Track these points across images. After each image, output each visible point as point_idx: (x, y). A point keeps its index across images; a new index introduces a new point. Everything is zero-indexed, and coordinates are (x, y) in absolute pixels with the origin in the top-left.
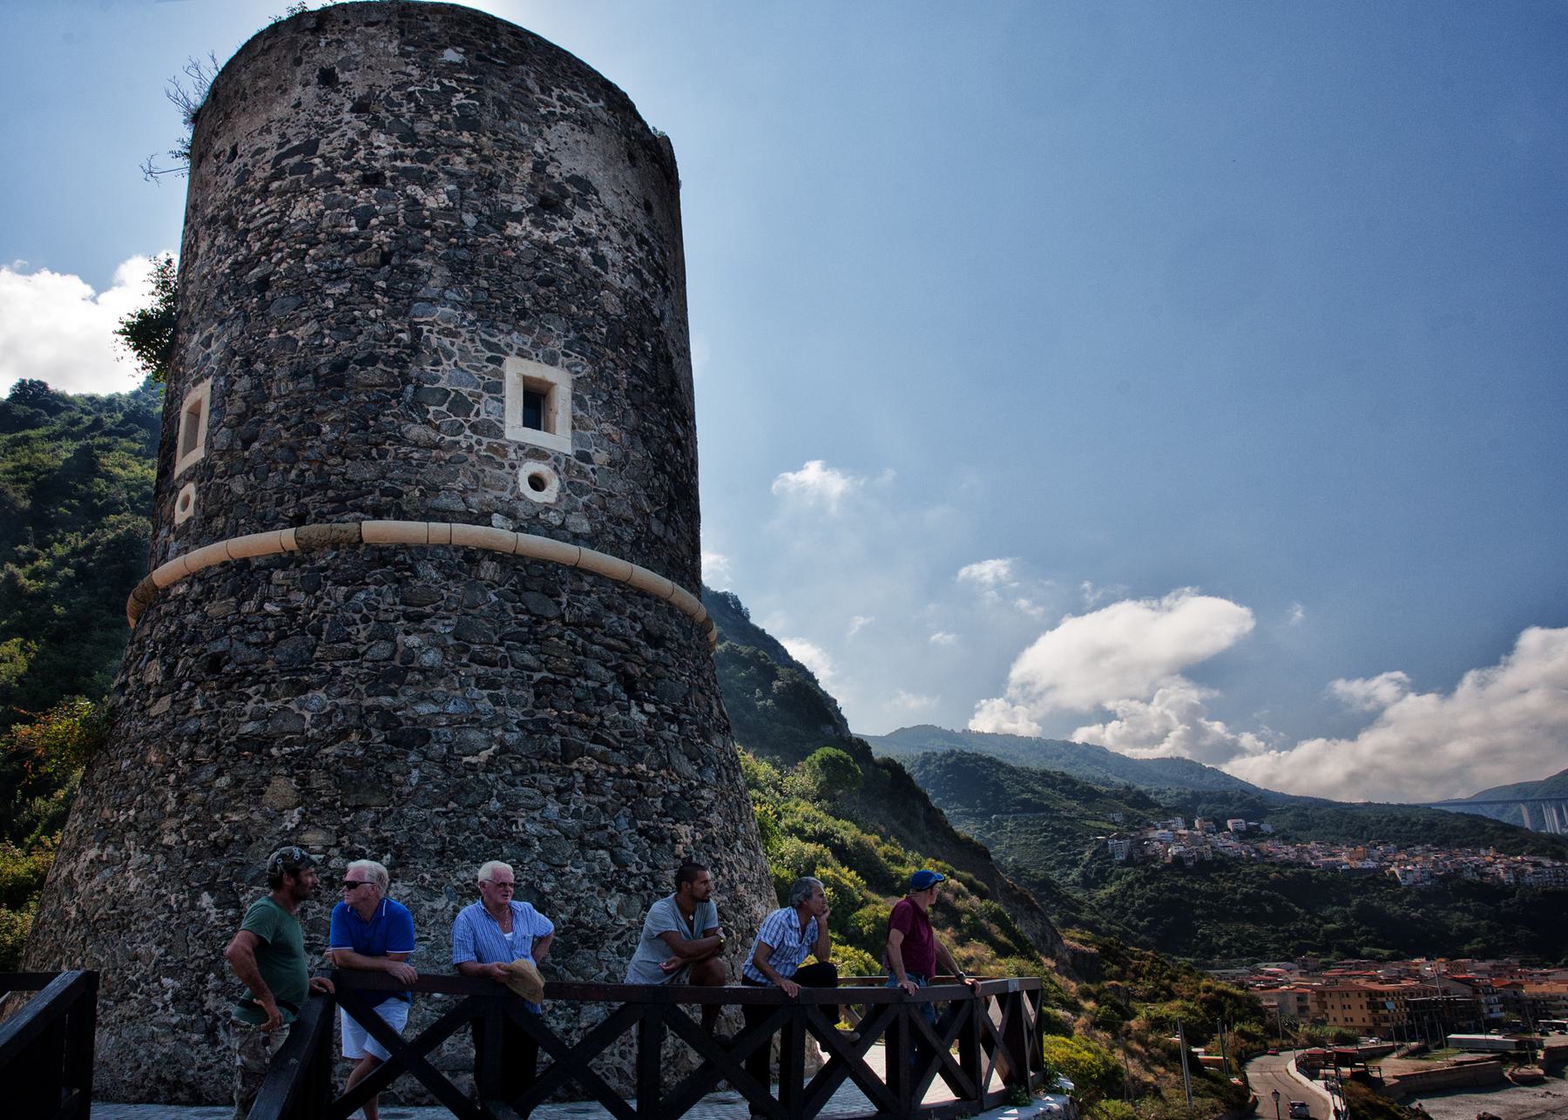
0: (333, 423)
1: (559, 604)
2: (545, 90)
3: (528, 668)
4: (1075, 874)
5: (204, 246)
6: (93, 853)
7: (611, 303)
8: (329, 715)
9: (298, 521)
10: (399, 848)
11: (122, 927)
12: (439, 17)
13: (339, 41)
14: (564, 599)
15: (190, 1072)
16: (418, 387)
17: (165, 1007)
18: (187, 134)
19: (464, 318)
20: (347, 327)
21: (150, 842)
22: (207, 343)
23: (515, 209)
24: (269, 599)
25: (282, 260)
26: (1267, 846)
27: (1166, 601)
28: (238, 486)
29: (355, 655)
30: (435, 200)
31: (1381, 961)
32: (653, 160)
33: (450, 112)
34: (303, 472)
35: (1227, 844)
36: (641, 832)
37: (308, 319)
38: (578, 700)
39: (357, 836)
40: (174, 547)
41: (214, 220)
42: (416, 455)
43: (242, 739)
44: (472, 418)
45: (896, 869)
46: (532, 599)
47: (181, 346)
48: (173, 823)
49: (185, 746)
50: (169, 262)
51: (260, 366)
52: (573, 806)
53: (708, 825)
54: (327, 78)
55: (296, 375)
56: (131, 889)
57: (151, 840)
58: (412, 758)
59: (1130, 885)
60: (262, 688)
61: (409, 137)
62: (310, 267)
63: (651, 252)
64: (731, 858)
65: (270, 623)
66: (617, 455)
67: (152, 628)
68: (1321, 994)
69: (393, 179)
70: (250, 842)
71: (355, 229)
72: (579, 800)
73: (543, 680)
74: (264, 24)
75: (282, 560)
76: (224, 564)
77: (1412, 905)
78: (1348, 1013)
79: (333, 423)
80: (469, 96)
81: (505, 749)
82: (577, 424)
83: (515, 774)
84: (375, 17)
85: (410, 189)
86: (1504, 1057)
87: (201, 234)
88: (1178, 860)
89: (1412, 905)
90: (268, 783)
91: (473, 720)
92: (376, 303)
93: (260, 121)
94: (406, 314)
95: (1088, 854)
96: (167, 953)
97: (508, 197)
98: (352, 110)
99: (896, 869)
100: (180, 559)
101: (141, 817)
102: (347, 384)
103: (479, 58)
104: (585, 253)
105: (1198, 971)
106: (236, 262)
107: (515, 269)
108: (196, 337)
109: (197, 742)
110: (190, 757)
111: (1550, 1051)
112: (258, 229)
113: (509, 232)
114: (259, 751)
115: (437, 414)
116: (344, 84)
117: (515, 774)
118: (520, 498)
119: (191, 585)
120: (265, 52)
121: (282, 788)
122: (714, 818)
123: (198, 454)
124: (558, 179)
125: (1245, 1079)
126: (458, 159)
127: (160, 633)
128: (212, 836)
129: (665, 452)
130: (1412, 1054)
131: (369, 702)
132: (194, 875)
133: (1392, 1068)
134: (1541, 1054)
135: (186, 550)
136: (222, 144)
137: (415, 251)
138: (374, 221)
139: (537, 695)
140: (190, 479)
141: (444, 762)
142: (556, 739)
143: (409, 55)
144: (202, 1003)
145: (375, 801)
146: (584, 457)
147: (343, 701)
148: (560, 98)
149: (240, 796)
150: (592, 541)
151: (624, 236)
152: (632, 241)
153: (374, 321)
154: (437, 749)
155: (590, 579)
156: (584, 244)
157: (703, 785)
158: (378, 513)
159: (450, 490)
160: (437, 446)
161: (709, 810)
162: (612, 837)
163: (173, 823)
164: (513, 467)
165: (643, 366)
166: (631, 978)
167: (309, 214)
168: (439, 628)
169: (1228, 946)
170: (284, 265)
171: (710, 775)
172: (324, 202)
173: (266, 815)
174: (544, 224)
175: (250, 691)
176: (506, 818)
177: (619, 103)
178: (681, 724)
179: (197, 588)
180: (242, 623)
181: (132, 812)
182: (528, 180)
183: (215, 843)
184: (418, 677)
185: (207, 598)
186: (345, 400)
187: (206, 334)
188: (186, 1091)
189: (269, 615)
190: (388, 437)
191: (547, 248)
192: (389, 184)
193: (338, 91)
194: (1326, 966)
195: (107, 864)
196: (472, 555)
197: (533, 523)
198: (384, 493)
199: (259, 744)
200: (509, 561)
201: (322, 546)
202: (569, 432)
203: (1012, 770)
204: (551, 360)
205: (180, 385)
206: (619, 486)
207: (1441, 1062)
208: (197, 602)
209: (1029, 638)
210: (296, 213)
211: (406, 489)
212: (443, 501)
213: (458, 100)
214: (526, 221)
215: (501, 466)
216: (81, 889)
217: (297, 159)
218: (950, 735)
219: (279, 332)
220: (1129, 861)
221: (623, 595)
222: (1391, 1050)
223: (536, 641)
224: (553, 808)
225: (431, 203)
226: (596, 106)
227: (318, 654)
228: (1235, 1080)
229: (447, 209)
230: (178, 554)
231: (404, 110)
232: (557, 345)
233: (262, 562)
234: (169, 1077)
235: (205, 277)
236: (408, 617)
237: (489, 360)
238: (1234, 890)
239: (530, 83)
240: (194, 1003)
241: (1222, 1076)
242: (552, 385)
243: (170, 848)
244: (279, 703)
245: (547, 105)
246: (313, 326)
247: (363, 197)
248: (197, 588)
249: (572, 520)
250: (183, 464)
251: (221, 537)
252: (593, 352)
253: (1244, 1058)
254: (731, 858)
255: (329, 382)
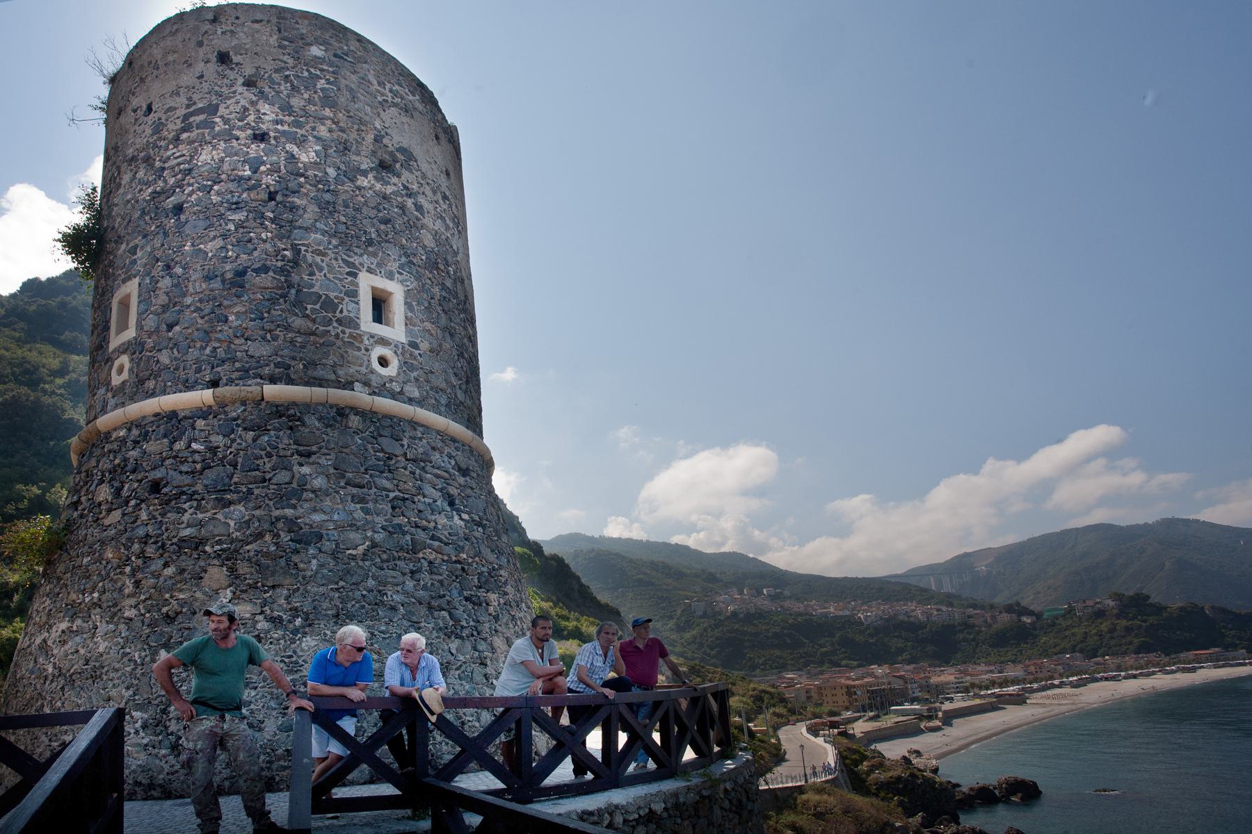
0: (237, 314)
1: (402, 446)
2: (381, 84)
3: (385, 489)
4: (671, 624)
5: (126, 178)
6: (64, 625)
7: (429, 241)
8: (248, 523)
9: (214, 384)
10: (307, 614)
11: (95, 677)
12: (306, 22)
13: (232, 32)
14: (405, 442)
15: (161, 777)
16: (298, 291)
17: (137, 732)
18: (105, 92)
19: (330, 243)
20: (245, 243)
21: (114, 614)
22: (133, 251)
23: (363, 167)
24: (195, 440)
25: (193, 192)
26: (787, 604)
27: (731, 451)
28: (164, 358)
29: (264, 480)
30: (307, 156)
31: (852, 668)
32: (450, 141)
33: (315, 92)
34: (215, 348)
35: (764, 603)
36: (467, 599)
37: (215, 238)
38: (420, 511)
39: (275, 606)
40: (112, 402)
41: (134, 159)
42: (299, 340)
43: (182, 540)
44: (338, 314)
45: (564, 623)
46: (386, 442)
47: (109, 253)
48: (132, 601)
49: (136, 546)
50: (94, 189)
51: (178, 270)
52: (422, 583)
53: (506, 594)
54: (223, 58)
55: (208, 278)
56: (101, 649)
57: (115, 614)
58: (312, 551)
59: (705, 630)
60: (195, 504)
61: (287, 108)
62: (215, 199)
63: (450, 205)
64: (521, 615)
65: (197, 457)
66: (435, 345)
67: (98, 461)
68: (819, 688)
69: (275, 138)
70: (195, 613)
71: (248, 173)
72: (426, 578)
73: (396, 498)
74: (172, 13)
75: (204, 412)
76: (156, 415)
77: (871, 636)
78: (835, 699)
79: (237, 314)
80: (328, 82)
81: (374, 545)
82: (408, 322)
83: (382, 561)
84: (259, 16)
85: (288, 147)
86: (921, 717)
87: (123, 169)
88: (734, 614)
89: (871, 636)
90: (206, 571)
91: (352, 525)
92: (266, 228)
93: (171, 86)
94: (289, 237)
95: (679, 612)
96: (135, 694)
97: (358, 158)
98: (244, 84)
99: (564, 623)
100: (120, 411)
101: (104, 598)
102: (247, 286)
103: (335, 55)
104: (409, 203)
105: (748, 679)
106: (155, 192)
107: (365, 210)
108: (123, 247)
109: (146, 543)
110: (141, 554)
111: (945, 712)
112: (172, 168)
113: (359, 183)
114: (197, 548)
115: (313, 310)
116: (237, 64)
117: (382, 561)
118: (372, 372)
119: (130, 430)
120: (173, 34)
121: (216, 574)
122: (509, 589)
123: (131, 333)
124: (391, 148)
125: (778, 740)
126: (323, 128)
127: (105, 464)
128: (165, 610)
129: (463, 344)
130: (871, 719)
131: (277, 513)
132: (152, 637)
133: (860, 728)
134: (940, 714)
135: (123, 405)
136: (139, 101)
137: (293, 192)
138: (263, 168)
139: (393, 508)
140: (124, 352)
141: (334, 555)
142: (408, 537)
143: (284, 47)
144: (166, 727)
145: (287, 581)
146: (414, 345)
147: (257, 513)
148: (391, 91)
149: (185, 581)
150: (420, 403)
151: (434, 192)
152: (439, 197)
153: (265, 241)
154: (328, 546)
155: (421, 429)
156: (409, 196)
157: (501, 567)
158: (273, 380)
159: (324, 365)
160: (313, 334)
161: (505, 583)
162: (448, 602)
163: (132, 601)
164: (367, 350)
165: (449, 283)
166: (499, 692)
167: (213, 159)
168: (323, 461)
169: (764, 664)
170: (194, 196)
171: (504, 560)
172: (224, 151)
173: (205, 593)
174: (382, 179)
175: (186, 506)
176: (380, 591)
177: (429, 98)
178: (484, 527)
179: (135, 432)
180: (175, 457)
181: (96, 595)
182: (371, 147)
183: (167, 615)
184: (311, 495)
185: (145, 439)
186: (246, 298)
187: (132, 244)
188: (159, 789)
189: (195, 452)
190: (278, 326)
191: (385, 197)
192: (273, 142)
193: (232, 69)
194: (822, 673)
195: (77, 633)
196: (342, 412)
197: (382, 389)
198: (277, 365)
199: (197, 544)
200: (369, 415)
201: (233, 403)
202: (403, 327)
203: (631, 561)
204: (390, 276)
205: (110, 282)
206: (437, 366)
207: (888, 721)
208: (136, 442)
209: (650, 476)
210: (202, 158)
211: (293, 363)
212: (320, 372)
213: (321, 84)
214: (370, 176)
215: (359, 349)
216: (55, 652)
217: (202, 117)
218: (592, 539)
219: (193, 245)
220: (705, 615)
221: (442, 441)
222: (860, 717)
223: (390, 471)
224: (410, 584)
225: (304, 158)
226: (415, 99)
227: (235, 479)
228: (773, 741)
229: (315, 163)
230: (116, 407)
231: (282, 88)
232: (393, 266)
233: (187, 413)
234: (144, 781)
235: (128, 201)
236: (301, 455)
237: (348, 274)
238: (767, 631)
239: (371, 78)
240: (160, 728)
241: (765, 739)
242: (391, 294)
243: (131, 620)
244: (209, 515)
245: (382, 95)
246: (219, 243)
247: (255, 150)
248: (135, 432)
249: (407, 388)
250: (115, 342)
251: (153, 395)
252: (417, 272)
253: (776, 728)
254: (521, 615)
255: (233, 284)
